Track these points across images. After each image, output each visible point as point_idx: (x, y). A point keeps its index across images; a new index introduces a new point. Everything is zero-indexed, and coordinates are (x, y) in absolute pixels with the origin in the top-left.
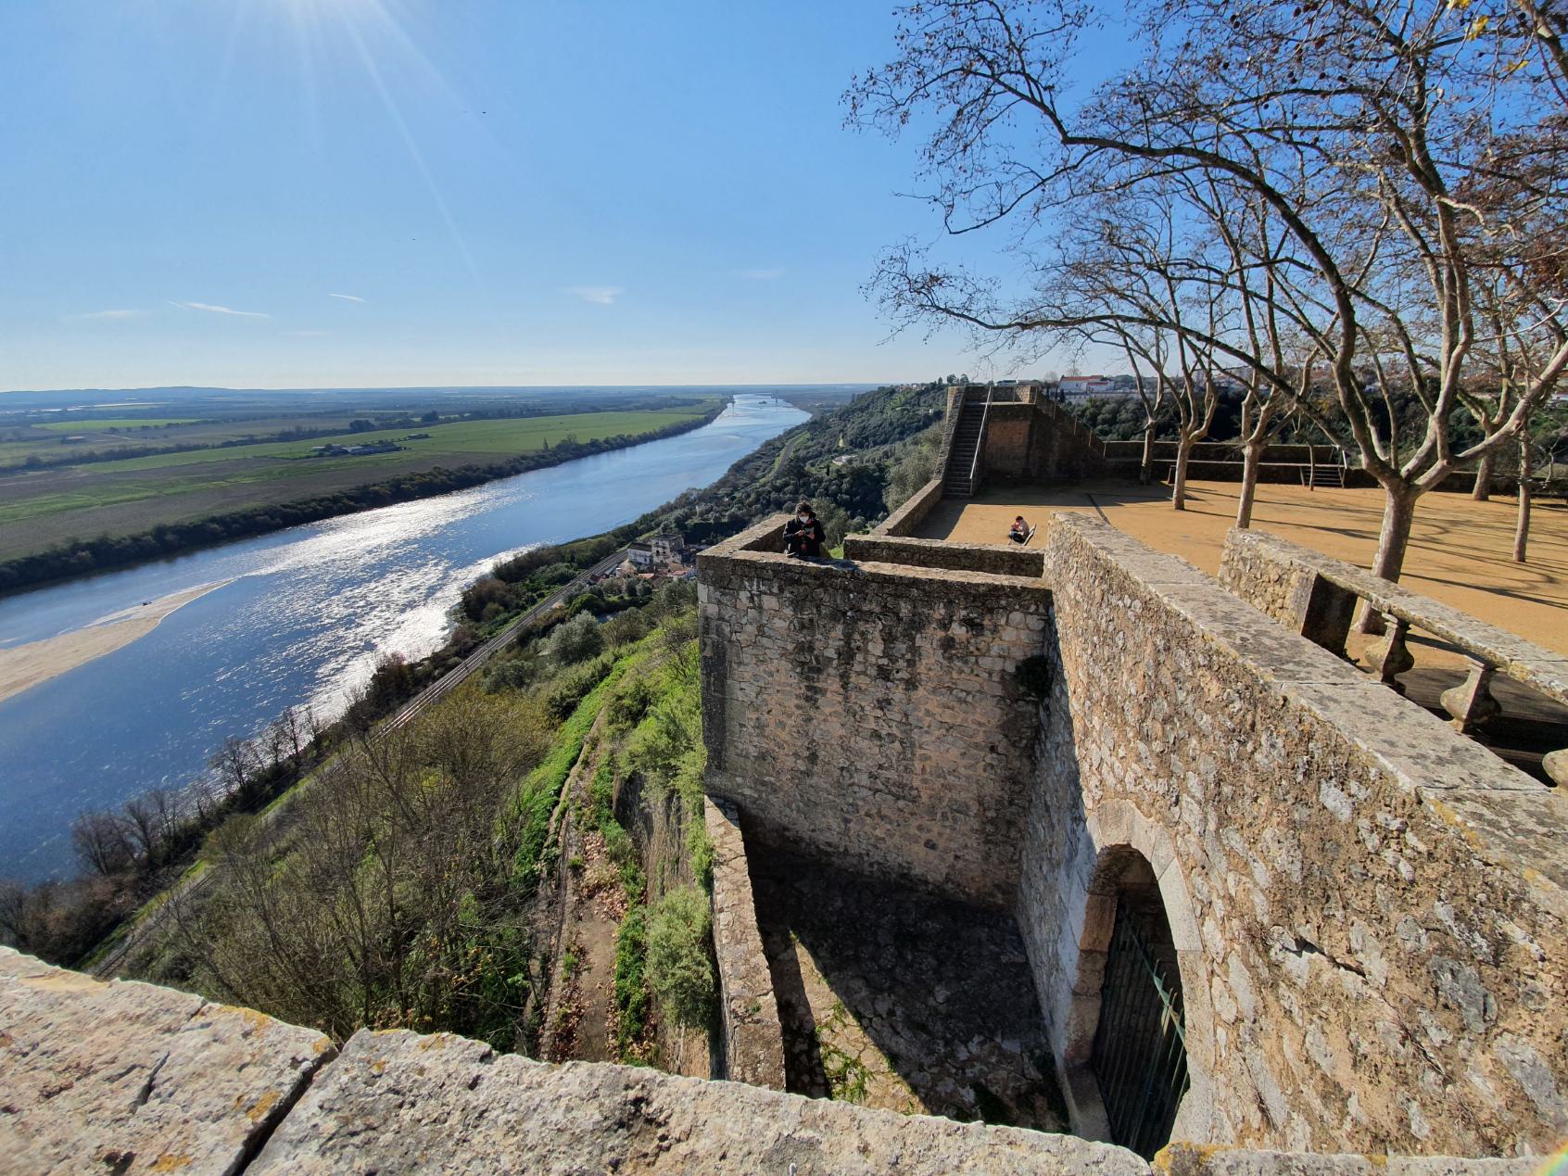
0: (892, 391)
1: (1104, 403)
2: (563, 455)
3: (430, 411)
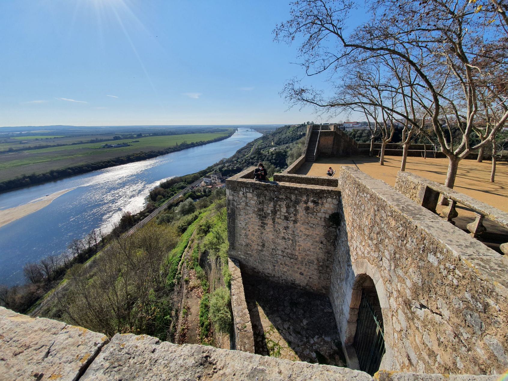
0: (289, 127)
1: (358, 131)
2: (182, 147)
3: (139, 133)
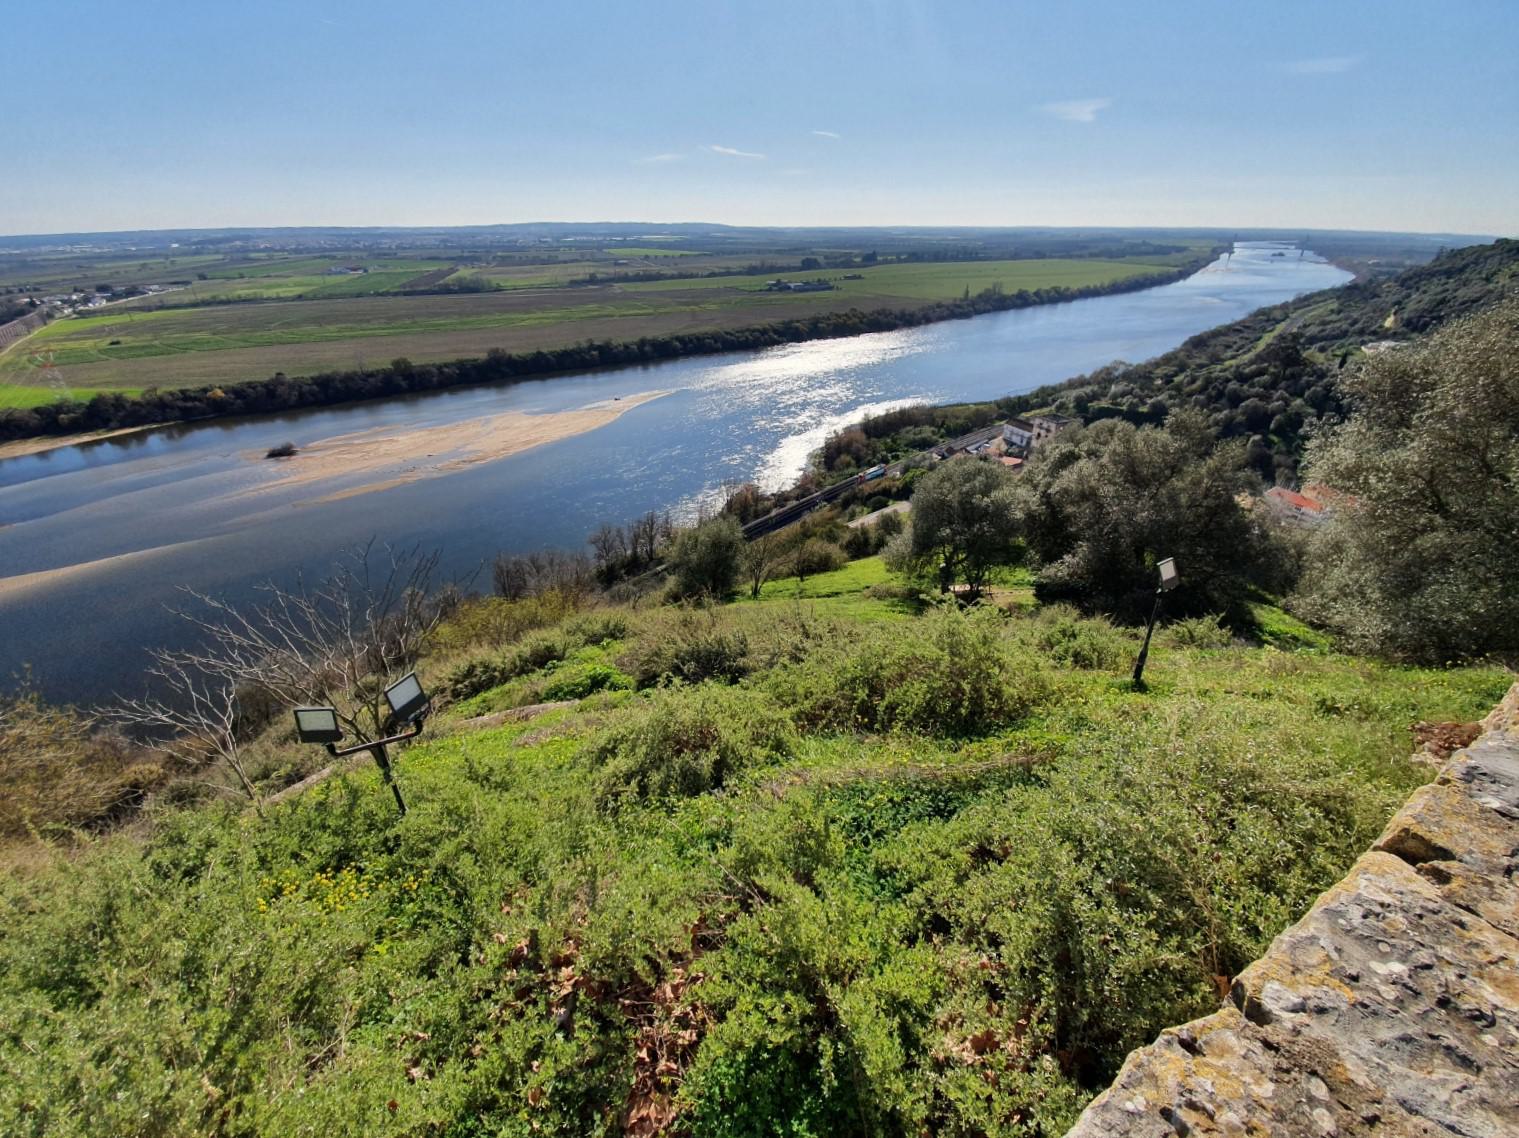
2: (981, 306)
